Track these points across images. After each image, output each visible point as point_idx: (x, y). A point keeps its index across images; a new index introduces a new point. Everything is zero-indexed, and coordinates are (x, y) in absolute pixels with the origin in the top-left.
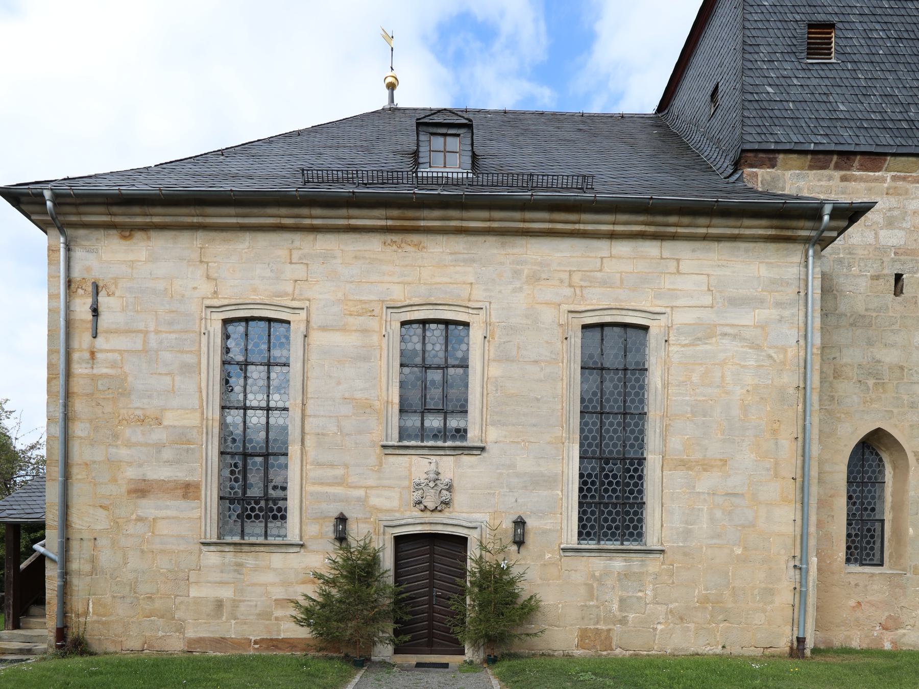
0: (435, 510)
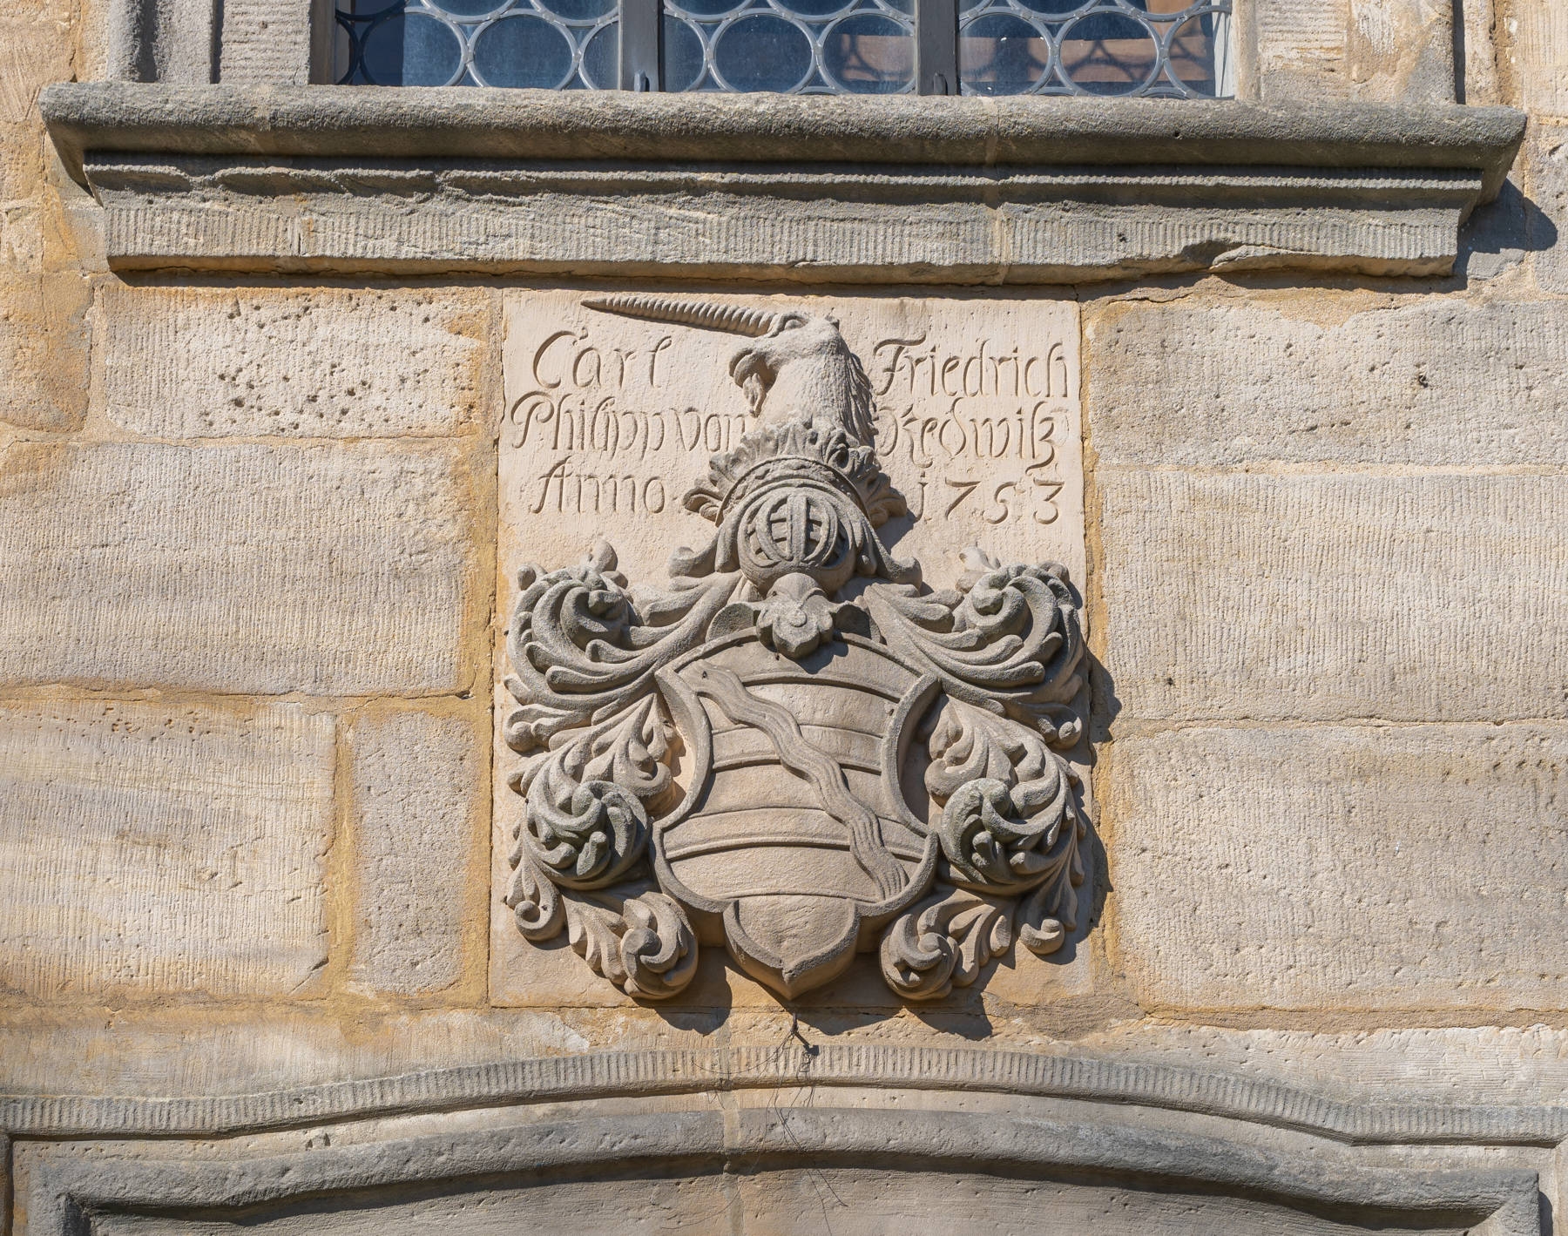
0: (839, 989)
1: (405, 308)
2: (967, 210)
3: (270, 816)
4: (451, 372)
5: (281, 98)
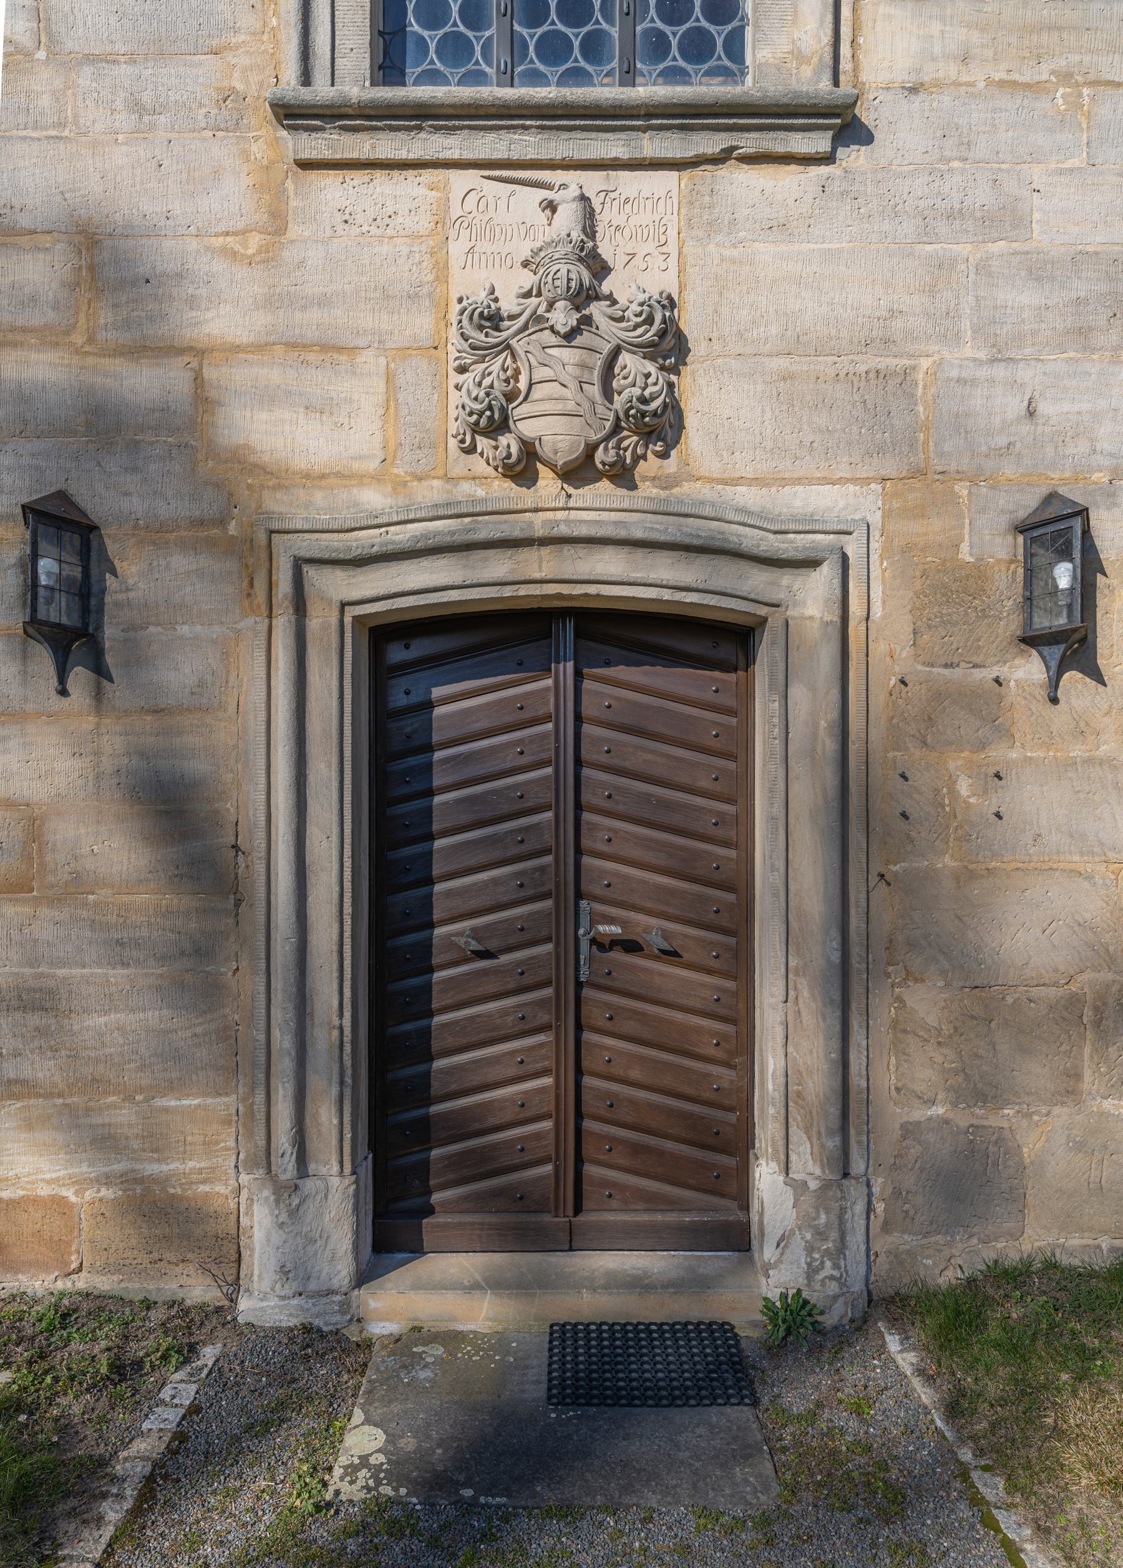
0: (579, 471)
1: (411, 179)
2: (633, 134)
3: (363, 400)
4: (429, 208)
5: (362, 94)
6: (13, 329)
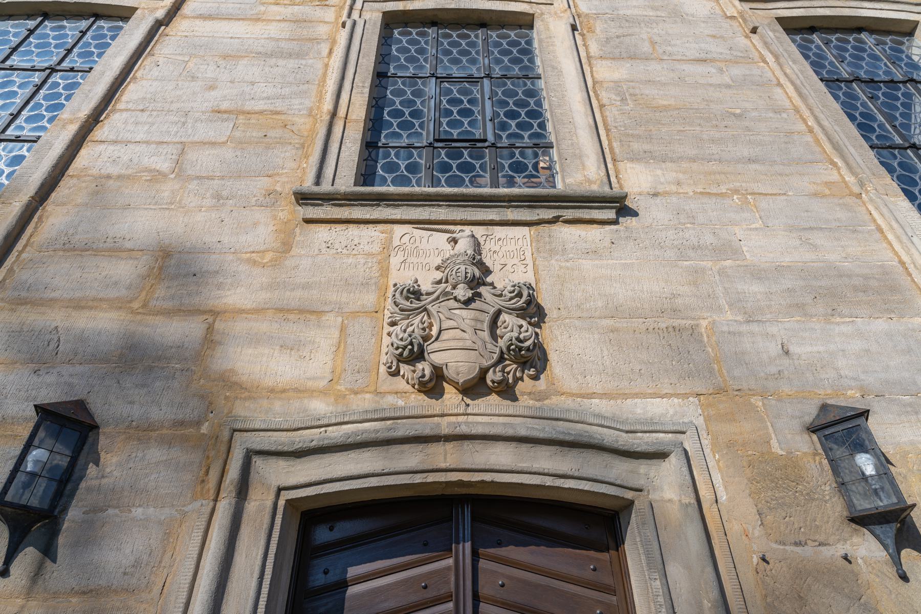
0: (475, 388)
6: (94, 300)
